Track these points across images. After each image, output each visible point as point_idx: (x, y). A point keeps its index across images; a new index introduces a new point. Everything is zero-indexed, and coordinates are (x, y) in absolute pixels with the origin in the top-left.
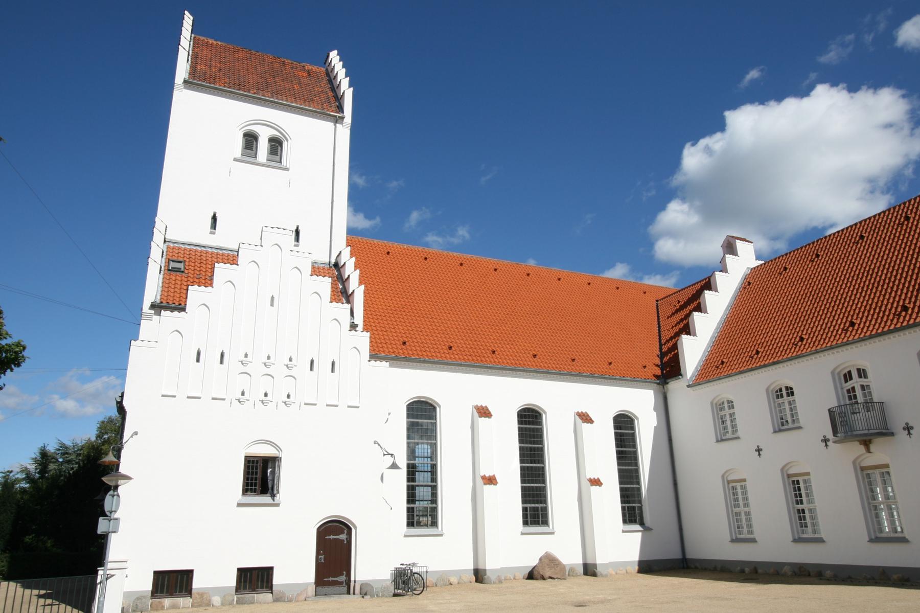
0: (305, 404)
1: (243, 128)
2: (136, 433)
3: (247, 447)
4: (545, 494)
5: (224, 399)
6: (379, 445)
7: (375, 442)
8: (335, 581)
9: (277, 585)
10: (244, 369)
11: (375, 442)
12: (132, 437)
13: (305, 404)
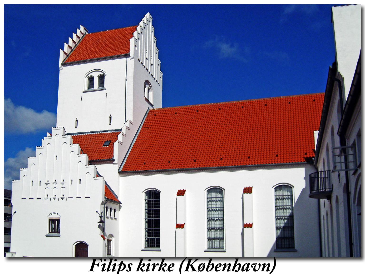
0: (69, 198)
1: (87, 75)
2: (15, 212)
3: (51, 214)
4: (85, 257)
5: (40, 198)
6: (98, 213)
7: (96, 212)
8: (358, 198)
9: (103, 256)
10: (47, 187)
11: (96, 212)
12: (14, 213)
13: (69, 198)
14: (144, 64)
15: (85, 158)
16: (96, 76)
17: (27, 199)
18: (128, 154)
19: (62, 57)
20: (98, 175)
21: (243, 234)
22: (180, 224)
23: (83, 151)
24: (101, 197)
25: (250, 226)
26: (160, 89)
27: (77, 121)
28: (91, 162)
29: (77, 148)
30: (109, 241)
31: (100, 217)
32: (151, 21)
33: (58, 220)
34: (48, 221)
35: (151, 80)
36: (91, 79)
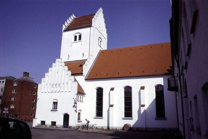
14: (98, 30)
15: (70, 73)
16: (78, 35)
17: (44, 92)
18: (90, 71)
19: (64, 28)
20: (75, 80)
21: (109, 94)
22: (112, 105)
23: (69, 69)
24: (76, 92)
25: (144, 106)
26: (106, 41)
27: (83, 54)
28: (72, 75)
29: (66, 68)
30: (79, 114)
31: (75, 101)
32: (102, 11)
33: (57, 103)
34: (52, 103)
35: (102, 37)
36: (76, 37)
